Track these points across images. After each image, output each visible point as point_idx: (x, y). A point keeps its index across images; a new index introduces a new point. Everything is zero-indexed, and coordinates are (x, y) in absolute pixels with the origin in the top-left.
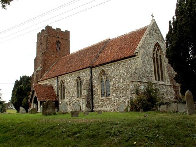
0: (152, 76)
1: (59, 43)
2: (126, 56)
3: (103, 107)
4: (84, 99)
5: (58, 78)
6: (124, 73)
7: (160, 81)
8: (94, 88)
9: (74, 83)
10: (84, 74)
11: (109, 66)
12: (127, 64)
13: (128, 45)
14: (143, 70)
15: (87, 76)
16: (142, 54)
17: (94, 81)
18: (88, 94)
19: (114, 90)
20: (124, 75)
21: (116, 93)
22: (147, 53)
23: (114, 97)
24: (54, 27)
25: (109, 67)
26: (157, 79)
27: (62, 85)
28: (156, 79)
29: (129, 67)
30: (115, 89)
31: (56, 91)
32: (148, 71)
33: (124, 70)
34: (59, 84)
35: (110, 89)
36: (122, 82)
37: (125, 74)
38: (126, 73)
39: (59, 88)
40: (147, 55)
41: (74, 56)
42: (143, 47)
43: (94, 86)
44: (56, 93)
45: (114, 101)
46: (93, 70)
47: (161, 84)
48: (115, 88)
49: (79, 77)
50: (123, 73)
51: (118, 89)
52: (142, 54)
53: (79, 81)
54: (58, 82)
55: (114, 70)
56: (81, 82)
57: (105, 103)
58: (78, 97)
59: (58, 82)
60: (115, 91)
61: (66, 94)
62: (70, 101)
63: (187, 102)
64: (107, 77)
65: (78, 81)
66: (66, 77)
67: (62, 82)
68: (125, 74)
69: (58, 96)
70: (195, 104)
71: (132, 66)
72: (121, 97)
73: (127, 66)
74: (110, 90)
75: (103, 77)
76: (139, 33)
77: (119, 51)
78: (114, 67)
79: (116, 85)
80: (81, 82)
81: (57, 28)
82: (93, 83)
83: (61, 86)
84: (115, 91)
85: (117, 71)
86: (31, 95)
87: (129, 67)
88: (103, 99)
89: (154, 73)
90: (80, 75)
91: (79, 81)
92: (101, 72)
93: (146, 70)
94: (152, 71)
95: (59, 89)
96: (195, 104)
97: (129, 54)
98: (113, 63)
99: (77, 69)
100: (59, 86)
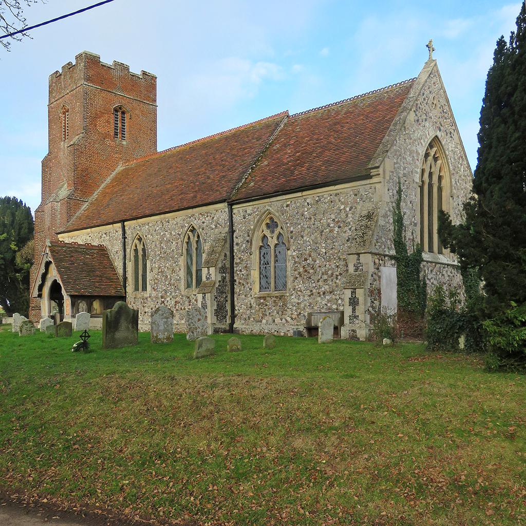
3: (264, 321)
5: (124, 227)
6: (332, 225)
19: (299, 273)
23: (299, 293)
24: (107, 60)
29: (348, 209)
30: (301, 270)
35: (289, 269)
45: (298, 304)
62: (162, 297)
67: (140, 239)
69: (125, 279)
73: (342, 207)
79: (306, 260)
94: (415, 225)
98: (299, 194)
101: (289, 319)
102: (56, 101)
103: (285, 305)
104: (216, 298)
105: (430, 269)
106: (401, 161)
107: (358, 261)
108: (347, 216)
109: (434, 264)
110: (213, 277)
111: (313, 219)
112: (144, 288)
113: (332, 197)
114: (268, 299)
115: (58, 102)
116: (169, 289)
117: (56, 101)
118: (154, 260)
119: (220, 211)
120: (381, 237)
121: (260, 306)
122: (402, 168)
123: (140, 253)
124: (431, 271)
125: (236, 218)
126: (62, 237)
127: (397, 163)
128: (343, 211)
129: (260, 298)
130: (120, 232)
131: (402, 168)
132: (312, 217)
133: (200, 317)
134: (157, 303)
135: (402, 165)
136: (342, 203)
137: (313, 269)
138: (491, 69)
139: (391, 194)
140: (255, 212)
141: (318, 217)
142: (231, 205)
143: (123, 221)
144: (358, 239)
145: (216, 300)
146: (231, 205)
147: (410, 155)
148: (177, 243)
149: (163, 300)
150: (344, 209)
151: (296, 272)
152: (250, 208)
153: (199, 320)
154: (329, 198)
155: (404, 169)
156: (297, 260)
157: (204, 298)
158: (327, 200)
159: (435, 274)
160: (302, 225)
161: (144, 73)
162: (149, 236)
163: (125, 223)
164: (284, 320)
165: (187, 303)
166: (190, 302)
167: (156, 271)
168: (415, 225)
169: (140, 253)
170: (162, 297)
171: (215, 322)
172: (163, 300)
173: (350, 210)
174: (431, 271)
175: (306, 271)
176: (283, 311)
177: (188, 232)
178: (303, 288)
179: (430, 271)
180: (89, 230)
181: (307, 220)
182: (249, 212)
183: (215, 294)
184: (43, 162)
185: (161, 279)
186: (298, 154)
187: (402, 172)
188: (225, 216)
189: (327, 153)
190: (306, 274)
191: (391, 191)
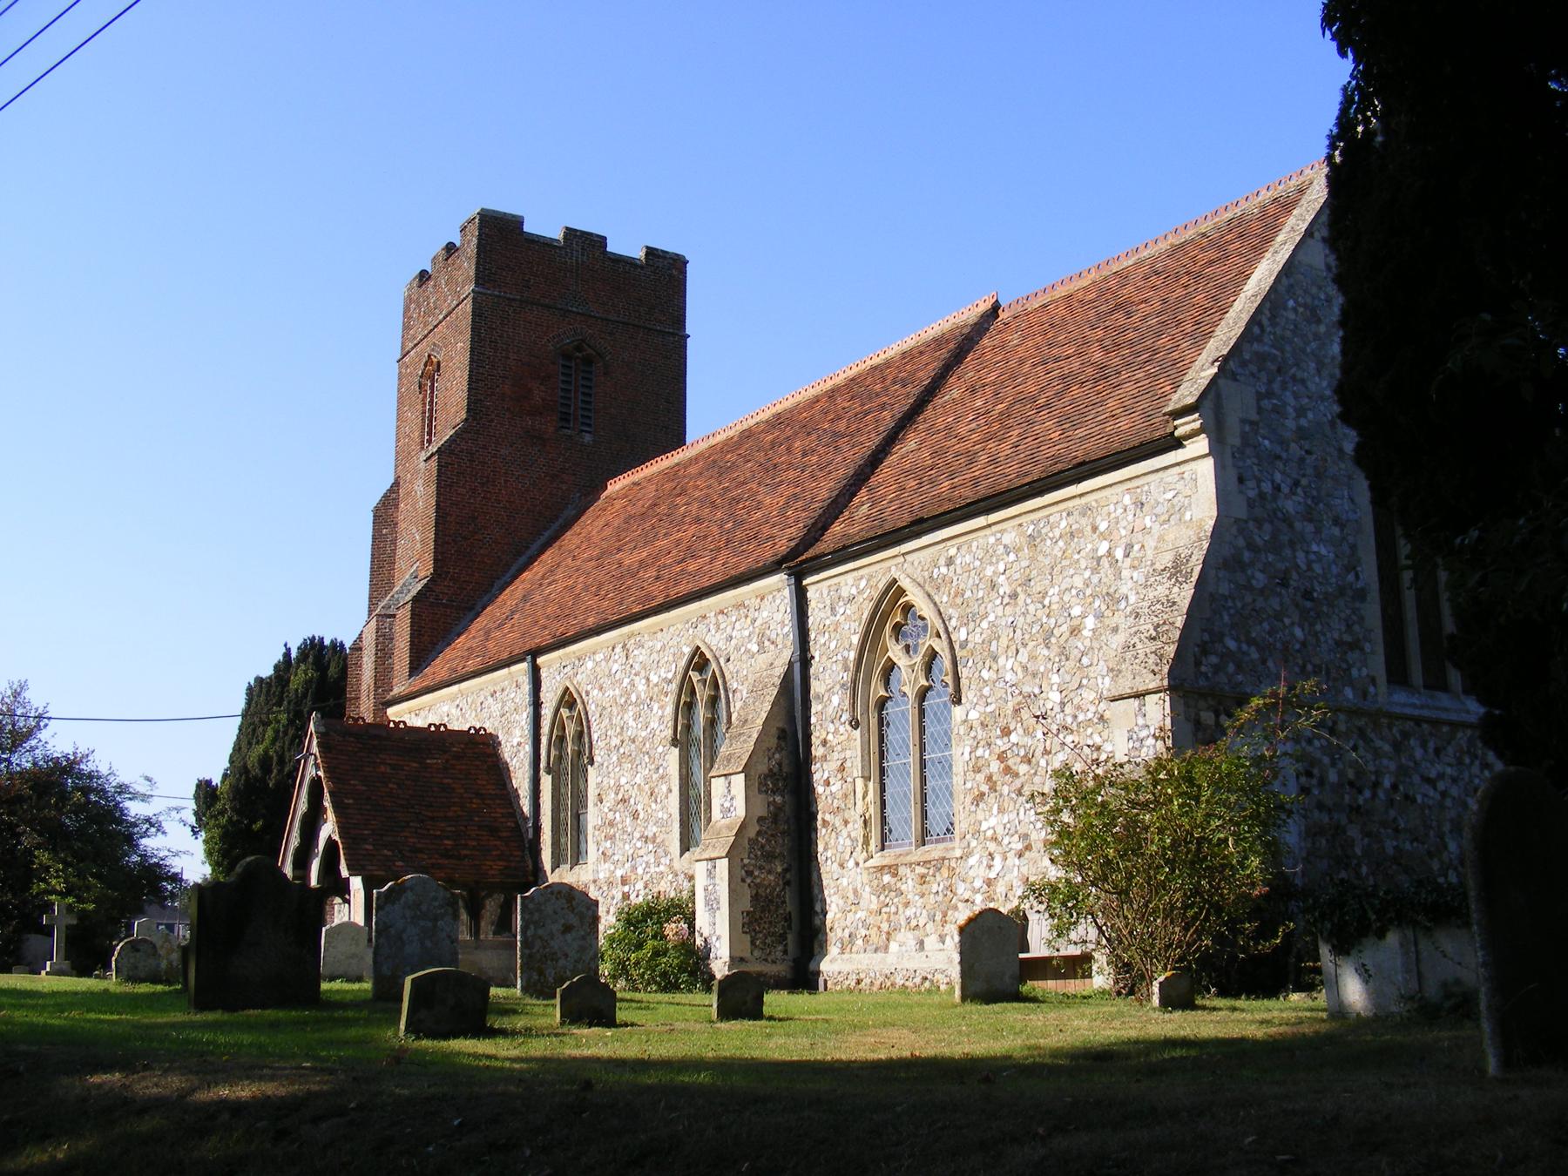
0: (1355, 645)
1: (588, 361)
2: (1093, 448)
3: (893, 946)
4: (723, 865)
5: (535, 672)
6: (1076, 611)
7: (1445, 688)
8: (824, 758)
9: (661, 718)
10: (742, 630)
11: (953, 551)
12: (1103, 526)
13: (1132, 344)
14: (1260, 580)
15: (762, 649)
16: (1243, 421)
17: (818, 697)
18: (761, 820)
19: (989, 778)
20: (1075, 631)
21: (1001, 811)
22: (1301, 412)
23: (992, 846)
24: (545, 223)
25: (950, 562)
26: (1417, 675)
27: (571, 729)
28: (1397, 675)
29: (1119, 554)
30: (995, 766)
31: (521, 780)
32: (1307, 595)
33: (1078, 582)
34: (545, 729)
35: (958, 768)
36: (1055, 697)
37: (1090, 622)
38: (1100, 616)
39: (543, 764)
40: (1302, 433)
41: (693, 470)
42: (1261, 358)
43: (824, 743)
44: (526, 806)
45: (989, 882)
46: (819, 588)
47: (1454, 717)
48: (1002, 757)
49: (699, 661)
50: (1065, 608)
51: (1023, 769)
52: (1243, 421)
53: (702, 694)
54: (537, 704)
55: (993, 586)
56: (713, 701)
57: (907, 904)
58: (685, 847)
59: (537, 704)
60: (993, 789)
61: (593, 817)
62: (624, 881)
63: (170, 992)
64: (933, 655)
65: (693, 692)
66: (599, 657)
67: (571, 704)
68: (1090, 622)
69: (537, 828)
70: (826, 989)
71: (1151, 543)
72: (611, 824)
73: (1103, 548)
74: (957, 780)
75: (895, 652)
76: (1241, 235)
77: (1047, 405)
78: (989, 555)
79: (1006, 732)
80: (713, 701)
81: (570, 233)
82: (816, 708)
83: (562, 739)
84: (993, 789)
85: (1014, 596)
86: (297, 824)
87: (1119, 554)
88: (893, 870)
89: (1372, 611)
90: (713, 641)
91: (702, 694)
92: (877, 606)
93: (1284, 583)
94: (1361, 595)
95: (542, 773)
96: (826, 989)
97: (1127, 429)
98: (981, 521)
99: (683, 589)
100: (544, 740)
102: (417, 345)
104: (749, 873)
105: (1431, 745)
106: (1284, 389)
107: (1141, 721)
108: (1118, 576)
109: (1445, 729)
111: (1022, 597)
113: (1071, 519)
114: (902, 871)
115: (418, 349)
116: (641, 852)
117: (417, 345)
118: (605, 764)
119: (770, 597)
120: (1222, 635)
121: (882, 897)
122: (1290, 410)
124: (1437, 751)
126: (395, 714)
127: (1270, 394)
128: (1105, 562)
130: (526, 687)
131: (1290, 410)
132: (1019, 590)
133: (574, 920)
135: (1292, 401)
136: (1103, 537)
137: (1029, 762)
139: (1252, 494)
141: (1036, 587)
142: (798, 575)
143: (536, 653)
144: (1139, 646)
145: (748, 881)
146: (798, 575)
147: (1319, 371)
149: (626, 889)
150: (1109, 553)
151: (980, 777)
152: (850, 578)
153: (568, 929)
154: (1063, 524)
155: (1301, 412)
156: (981, 734)
158: (1057, 533)
159: (1453, 761)
160: (992, 617)
161: (651, 252)
162: (596, 692)
163: (540, 660)
167: (610, 799)
168: (1361, 595)
170: (624, 881)
171: (747, 955)
172: (626, 889)
173: (1127, 556)
174: (1437, 751)
175: (1008, 770)
177: (690, 673)
178: (1000, 830)
179: (1431, 751)
180: (455, 688)
181: (1006, 600)
182: (845, 593)
183: (746, 861)
184: (376, 511)
186: (1000, 406)
187: (1290, 423)
189: (1076, 391)
191: (1251, 484)
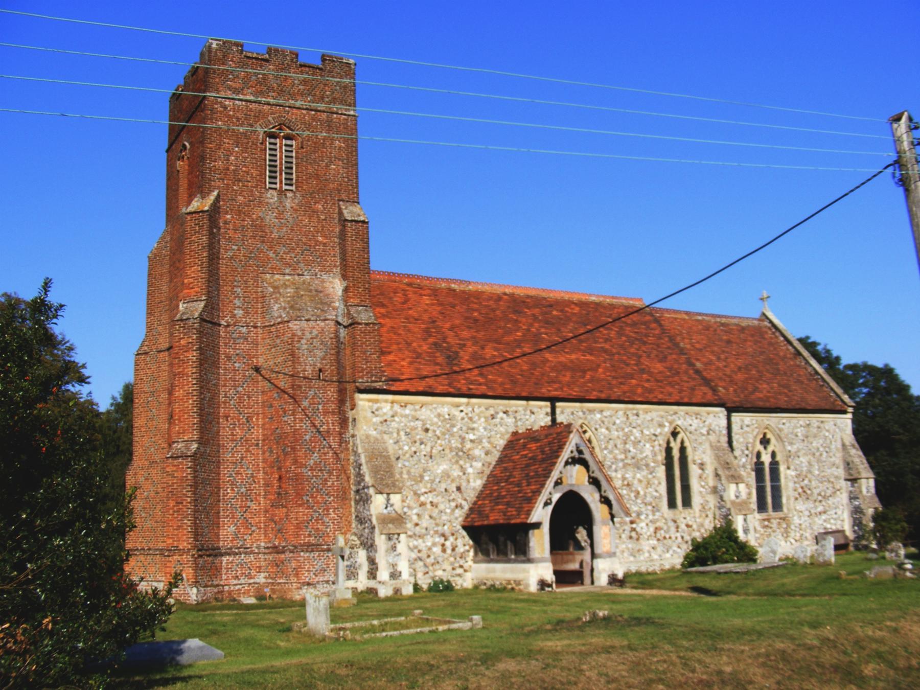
30: (800, 490)
101: (793, 541)
103: (788, 526)
110: (744, 496)
112: (687, 503)
123: (676, 454)
125: (735, 428)
129: (764, 520)
132: (643, 441)
134: (624, 530)
138: (512, 295)
140: (753, 424)
148: (653, 447)
152: (748, 419)
157: (745, 520)
164: (789, 543)
165: (673, 529)
166: (677, 527)
169: (676, 454)
175: (804, 492)
176: (786, 534)
185: (629, 495)
188: (724, 422)
190: (804, 494)
